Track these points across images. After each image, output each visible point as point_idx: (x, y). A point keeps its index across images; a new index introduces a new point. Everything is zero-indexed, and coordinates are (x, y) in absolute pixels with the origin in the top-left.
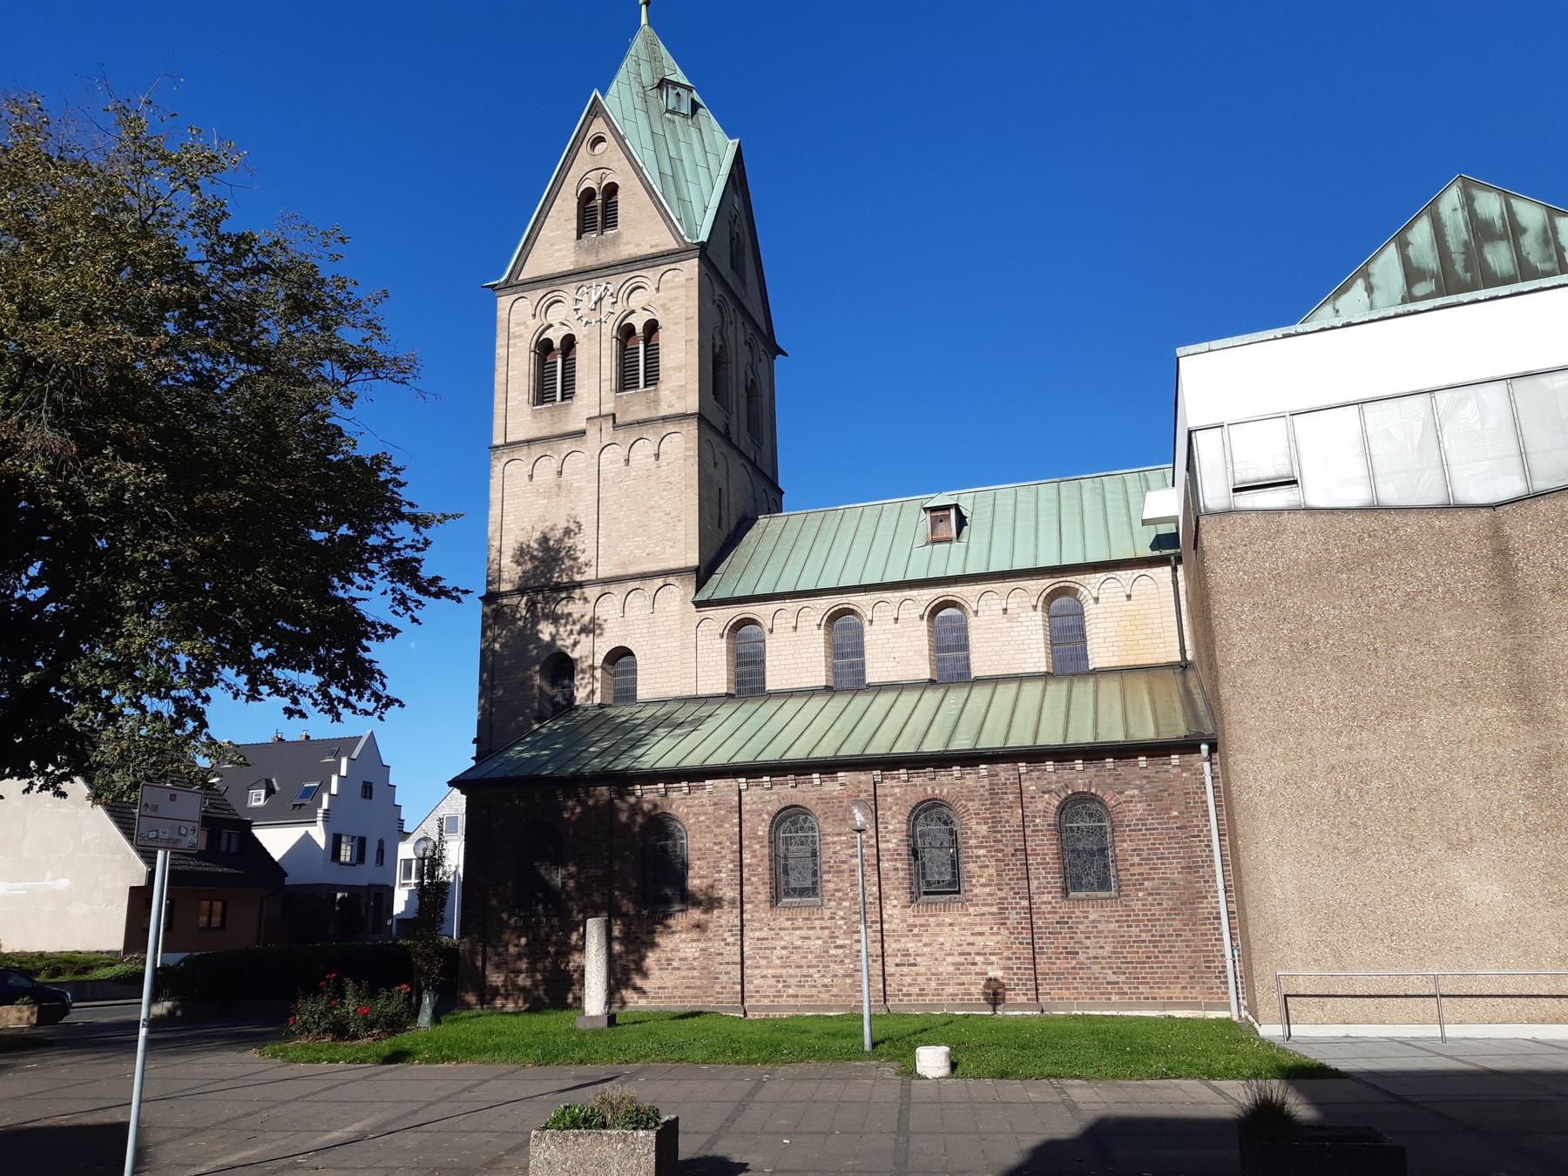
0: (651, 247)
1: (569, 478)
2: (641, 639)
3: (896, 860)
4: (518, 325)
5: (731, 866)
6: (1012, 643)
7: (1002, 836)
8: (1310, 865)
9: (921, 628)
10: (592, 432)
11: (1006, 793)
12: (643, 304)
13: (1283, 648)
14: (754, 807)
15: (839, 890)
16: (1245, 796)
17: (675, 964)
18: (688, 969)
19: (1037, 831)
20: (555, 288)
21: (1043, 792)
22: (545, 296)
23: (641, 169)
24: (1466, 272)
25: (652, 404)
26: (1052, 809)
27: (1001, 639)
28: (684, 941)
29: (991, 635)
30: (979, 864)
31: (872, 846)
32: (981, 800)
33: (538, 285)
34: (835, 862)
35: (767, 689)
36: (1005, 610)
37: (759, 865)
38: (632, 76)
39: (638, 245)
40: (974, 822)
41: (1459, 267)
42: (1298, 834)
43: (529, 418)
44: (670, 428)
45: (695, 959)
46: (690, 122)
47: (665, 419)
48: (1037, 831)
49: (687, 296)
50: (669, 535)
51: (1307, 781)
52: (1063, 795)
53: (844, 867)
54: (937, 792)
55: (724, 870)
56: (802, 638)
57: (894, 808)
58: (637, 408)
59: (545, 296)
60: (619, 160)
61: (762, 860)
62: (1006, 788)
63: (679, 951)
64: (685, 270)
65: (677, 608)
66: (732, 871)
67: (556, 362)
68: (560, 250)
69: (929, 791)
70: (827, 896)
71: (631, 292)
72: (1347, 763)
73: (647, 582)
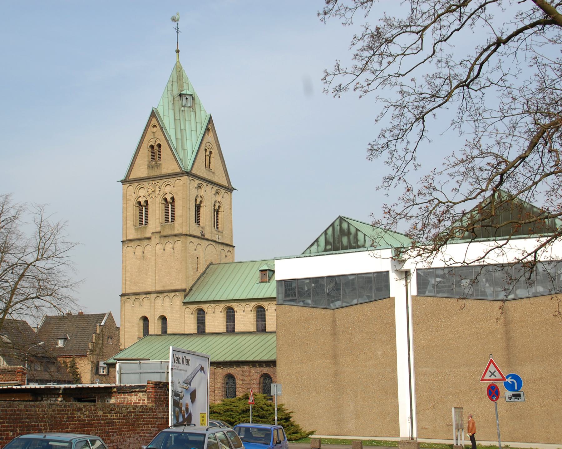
0: (172, 170)
1: (147, 254)
20: (141, 183)
21: (256, 373)
24: (338, 244)
26: (258, 378)
29: (271, 318)
31: (213, 386)
33: (135, 182)
38: (169, 92)
40: (239, 380)
41: (336, 242)
42: (289, 388)
43: (134, 231)
44: (177, 238)
46: (191, 109)
50: (177, 277)
52: (261, 374)
57: (219, 376)
58: (167, 230)
65: (179, 303)
69: (228, 371)
71: (166, 186)
72: (300, 372)
73: (170, 293)
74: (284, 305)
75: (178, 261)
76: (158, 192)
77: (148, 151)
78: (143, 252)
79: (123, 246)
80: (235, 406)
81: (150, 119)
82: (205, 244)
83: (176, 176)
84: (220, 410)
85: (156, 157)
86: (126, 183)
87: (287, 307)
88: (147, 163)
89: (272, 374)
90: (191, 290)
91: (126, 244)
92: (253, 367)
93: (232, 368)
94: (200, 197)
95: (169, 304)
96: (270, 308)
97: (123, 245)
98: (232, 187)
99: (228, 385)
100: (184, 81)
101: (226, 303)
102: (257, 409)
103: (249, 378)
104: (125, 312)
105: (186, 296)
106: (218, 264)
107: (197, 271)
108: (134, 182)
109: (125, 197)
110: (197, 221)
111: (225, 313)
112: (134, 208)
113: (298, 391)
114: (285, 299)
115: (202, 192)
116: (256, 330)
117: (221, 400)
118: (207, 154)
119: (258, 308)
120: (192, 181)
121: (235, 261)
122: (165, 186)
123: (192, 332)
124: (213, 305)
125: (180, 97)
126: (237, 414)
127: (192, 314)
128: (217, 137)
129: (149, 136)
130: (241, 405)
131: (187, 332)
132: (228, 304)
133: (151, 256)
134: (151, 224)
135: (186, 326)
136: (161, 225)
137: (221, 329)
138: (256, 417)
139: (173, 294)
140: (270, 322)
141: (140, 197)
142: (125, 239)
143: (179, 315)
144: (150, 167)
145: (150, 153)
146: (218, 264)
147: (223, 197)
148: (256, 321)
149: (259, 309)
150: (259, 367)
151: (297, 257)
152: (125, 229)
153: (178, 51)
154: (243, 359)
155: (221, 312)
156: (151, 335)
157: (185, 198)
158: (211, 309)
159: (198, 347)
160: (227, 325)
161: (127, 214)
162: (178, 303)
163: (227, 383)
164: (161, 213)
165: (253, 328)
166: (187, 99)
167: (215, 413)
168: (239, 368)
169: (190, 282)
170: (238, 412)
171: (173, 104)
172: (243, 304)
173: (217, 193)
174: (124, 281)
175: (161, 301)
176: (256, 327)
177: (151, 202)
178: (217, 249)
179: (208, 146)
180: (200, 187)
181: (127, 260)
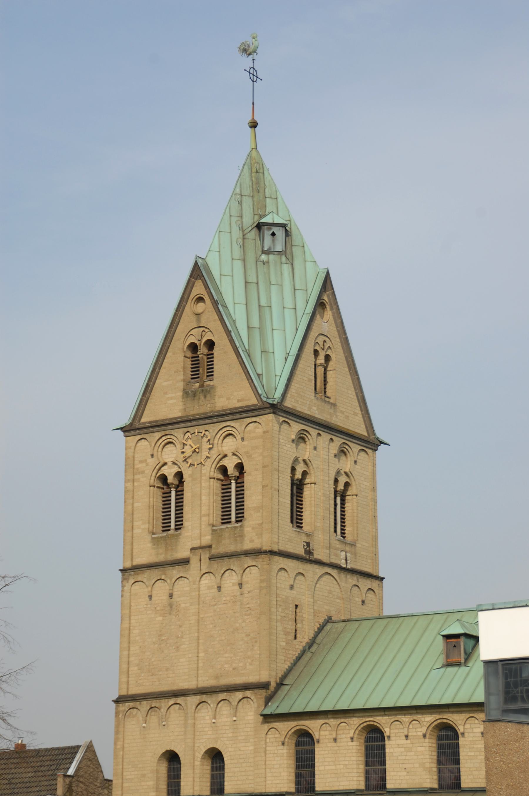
9: (424, 745)
10: (194, 561)
20: (167, 432)
22: (161, 438)
25: (238, 539)
29: (472, 754)
33: (155, 429)
35: (317, 789)
38: (234, 219)
39: (228, 399)
43: (150, 545)
44: (249, 561)
46: (284, 258)
47: (247, 553)
50: (249, 653)
58: (227, 541)
59: (161, 438)
64: (263, 424)
65: (252, 717)
68: (171, 398)
71: (225, 438)
78: (171, 596)
79: (125, 582)
81: (191, 284)
86: (132, 433)
87: (511, 728)
88: (181, 385)
90: (280, 684)
91: (131, 578)
94: (302, 462)
95: (229, 719)
97: (124, 579)
98: (378, 439)
100: (267, 195)
101: (364, 717)
105: (268, 700)
107: (295, 638)
111: (363, 741)
114: (506, 707)
115: (308, 450)
116: (436, 786)
118: (318, 362)
120: (285, 426)
122: (222, 437)
124: (333, 722)
125: (257, 231)
127: (283, 744)
128: (342, 322)
132: (369, 720)
133: (188, 605)
134: (190, 527)
136: (213, 531)
139: (239, 695)
140: (472, 765)
141: (165, 464)
142: (128, 565)
143: (252, 748)
145: (189, 362)
146: (344, 621)
148: (435, 761)
153: (254, 125)
155: (352, 738)
158: (327, 733)
160: (367, 772)
161: (136, 505)
164: (212, 501)
165: (428, 781)
166: (273, 234)
171: (243, 247)
173: (343, 451)
174: (125, 666)
175: (211, 713)
177: (191, 476)
178: (342, 584)
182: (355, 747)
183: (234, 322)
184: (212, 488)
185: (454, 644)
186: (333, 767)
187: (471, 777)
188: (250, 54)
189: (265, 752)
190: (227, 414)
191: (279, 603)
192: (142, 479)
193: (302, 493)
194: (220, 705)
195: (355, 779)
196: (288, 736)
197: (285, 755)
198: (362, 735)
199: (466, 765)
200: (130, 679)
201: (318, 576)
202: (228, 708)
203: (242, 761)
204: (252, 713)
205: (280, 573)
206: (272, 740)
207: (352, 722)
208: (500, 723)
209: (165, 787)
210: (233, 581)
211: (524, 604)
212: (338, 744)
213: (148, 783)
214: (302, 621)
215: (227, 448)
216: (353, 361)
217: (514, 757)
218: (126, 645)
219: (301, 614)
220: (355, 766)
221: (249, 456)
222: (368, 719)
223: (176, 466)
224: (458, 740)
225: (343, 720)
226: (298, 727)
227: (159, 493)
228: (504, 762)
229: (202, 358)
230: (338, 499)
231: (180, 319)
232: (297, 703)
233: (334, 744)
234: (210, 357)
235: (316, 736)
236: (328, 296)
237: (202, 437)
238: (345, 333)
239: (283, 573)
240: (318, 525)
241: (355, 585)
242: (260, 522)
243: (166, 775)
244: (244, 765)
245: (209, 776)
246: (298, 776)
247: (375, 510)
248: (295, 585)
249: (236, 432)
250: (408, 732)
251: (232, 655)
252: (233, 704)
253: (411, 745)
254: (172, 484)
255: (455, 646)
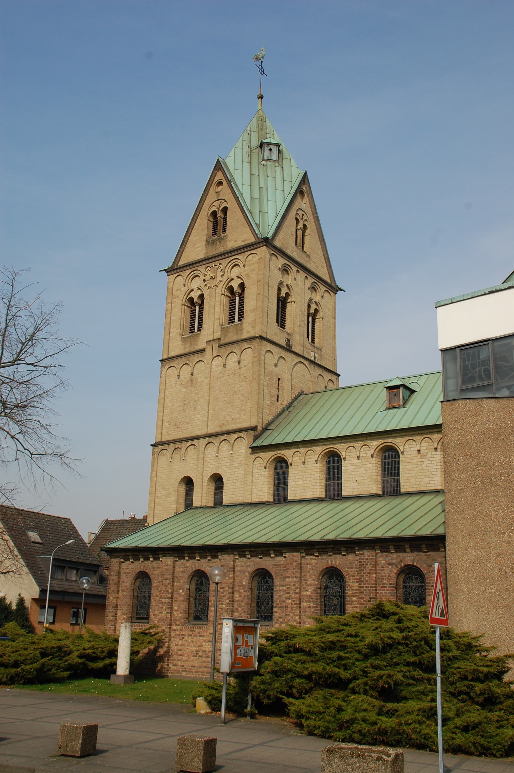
0: (242, 241)
2: (226, 469)
3: (310, 602)
4: (177, 290)
5: (228, 601)
6: (423, 471)
7: (364, 590)
8: (483, 613)
9: (372, 462)
10: (208, 350)
11: (367, 564)
12: (238, 274)
13: (479, 482)
14: (242, 568)
15: (280, 618)
16: (453, 571)
17: (200, 654)
18: (206, 657)
19: (384, 587)
20: (195, 269)
21: (389, 564)
23: (238, 198)
26: (393, 575)
27: (415, 469)
28: (205, 641)
29: (410, 467)
30: (353, 605)
31: (297, 593)
32: (356, 568)
33: (186, 268)
34: (280, 601)
36: (419, 451)
37: (242, 601)
38: (245, 143)
39: (236, 241)
43: (180, 343)
44: (246, 345)
45: (209, 652)
46: (277, 164)
47: (244, 340)
48: (384, 587)
49: (259, 268)
50: (243, 408)
51: (485, 562)
52: (399, 567)
53: (284, 604)
54: (333, 563)
55: (224, 603)
56: (308, 469)
57: (311, 572)
58: (231, 334)
60: (228, 194)
61: (244, 599)
62: (368, 562)
63: (202, 646)
65: (244, 451)
66: (228, 603)
67: (195, 310)
68: (198, 247)
69: (330, 562)
70: (274, 619)
71: (232, 268)
74: (463, 401)
75: (245, 381)
76: (219, 278)
77: (208, 220)
78: (192, 374)
79: (163, 368)
80: (351, 636)
81: (214, 174)
82: (293, 360)
83: (249, 249)
84: (310, 645)
85: (220, 227)
86: (172, 272)
87: (469, 405)
88: (205, 238)
89: (425, 566)
90: (265, 429)
91: (167, 365)
92: (382, 552)
93: (338, 556)
94: (285, 286)
95: (227, 453)
96: (409, 450)
97: (162, 366)
98: (337, 286)
99: (328, 590)
100: (267, 132)
101: (326, 445)
102: (415, 643)
103: (374, 575)
104: (158, 472)
105: (256, 438)
106: (312, 393)
107: (278, 400)
108: (184, 269)
109: (170, 293)
110: (281, 321)
111: (324, 463)
112: (183, 309)
113: (504, 599)
114: (463, 387)
115: (290, 279)
116: (380, 492)
117: (316, 619)
118: (298, 227)
119: (385, 452)
120: (274, 258)
121: (340, 386)
122: (230, 267)
123: (265, 499)
124: (302, 450)
125: (260, 150)
126: (357, 656)
127: (265, 467)
128: (315, 206)
129: (211, 197)
130: (368, 633)
131: (256, 499)
132: (330, 447)
133: (203, 379)
134: (207, 328)
135: (254, 490)
136: (222, 328)
137: (315, 493)
138: (411, 668)
139: (235, 436)
140: (410, 475)
141: (193, 290)
142: (165, 357)
143: (243, 472)
144: (209, 243)
145: (211, 224)
146: (312, 393)
147: (322, 297)
148: (380, 475)
149: (387, 454)
150: (396, 552)
151: (491, 292)
152: (168, 342)
153: (261, 97)
154: (362, 535)
155: (316, 461)
156: (196, 508)
157: (261, 281)
158: (298, 458)
159: (272, 520)
160: (327, 486)
161: (172, 318)
162: (242, 451)
163: (326, 587)
164: (222, 309)
165: (375, 488)
166: (270, 150)
167: (297, 650)
168: (353, 555)
169: (264, 416)
170: (359, 652)
171: (250, 156)
172: (358, 445)
173: (313, 288)
174: (160, 423)
175: (215, 450)
176: (380, 486)
177: (208, 295)
178: (312, 372)
179: (301, 216)
180: (287, 271)
181: (166, 388)
182: (318, 467)
183: (242, 194)
184: (222, 301)
185: (394, 393)
186: (302, 482)
187: (409, 484)
188: (260, 59)
189: (252, 474)
190: (234, 251)
191: (266, 374)
192: (177, 301)
193: (285, 309)
194: (222, 444)
195: (318, 490)
196: (269, 462)
197: (267, 475)
198: (324, 459)
199: (405, 475)
200: (163, 431)
201: (295, 362)
202: (228, 446)
203: (236, 481)
204: (244, 448)
205: (267, 354)
206: (257, 466)
207: (316, 449)
208: (458, 401)
209: (184, 502)
210: (234, 360)
211: (483, 293)
212: (306, 466)
213: (171, 499)
214: (283, 390)
215: (234, 274)
216: (322, 232)
217: (472, 429)
218: (162, 409)
219: (282, 385)
220: (318, 481)
221: (248, 275)
222: (329, 447)
223: (200, 291)
224: (399, 458)
225: (309, 449)
226: (277, 456)
227: (188, 311)
228: (461, 435)
229: (220, 219)
230: (310, 319)
231: (206, 197)
232: (276, 439)
233: (303, 466)
234: (225, 219)
235: (290, 461)
236: (306, 188)
237: (217, 269)
238: (317, 213)
239: (269, 354)
240: (296, 329)
241: (321, 375)
242: (255, 319)
243: (184, 494)
244: (237, 484)
245: (213, 493)
246: (276, 490)
247: (335, 331)
248: (278, 364)
249: (240, 262)
250: (360, 454)
251: (232, 410)
252: (231, 442)
253: (362, 464)
254: (197, 303)
255: (395, 395)
